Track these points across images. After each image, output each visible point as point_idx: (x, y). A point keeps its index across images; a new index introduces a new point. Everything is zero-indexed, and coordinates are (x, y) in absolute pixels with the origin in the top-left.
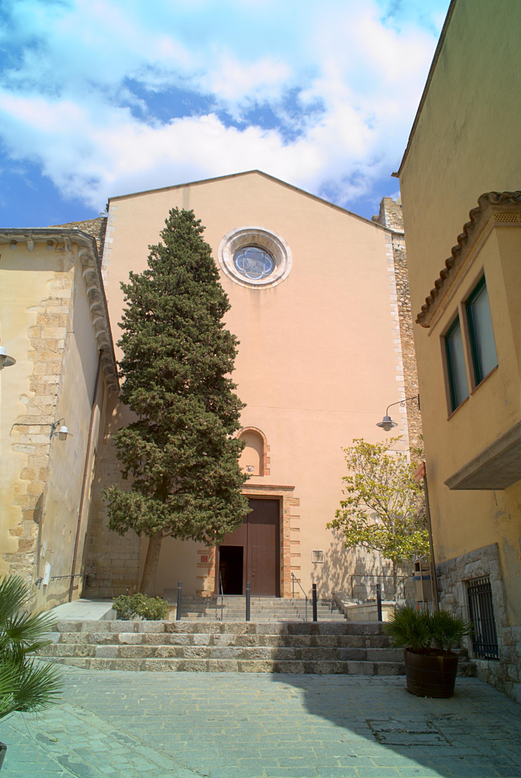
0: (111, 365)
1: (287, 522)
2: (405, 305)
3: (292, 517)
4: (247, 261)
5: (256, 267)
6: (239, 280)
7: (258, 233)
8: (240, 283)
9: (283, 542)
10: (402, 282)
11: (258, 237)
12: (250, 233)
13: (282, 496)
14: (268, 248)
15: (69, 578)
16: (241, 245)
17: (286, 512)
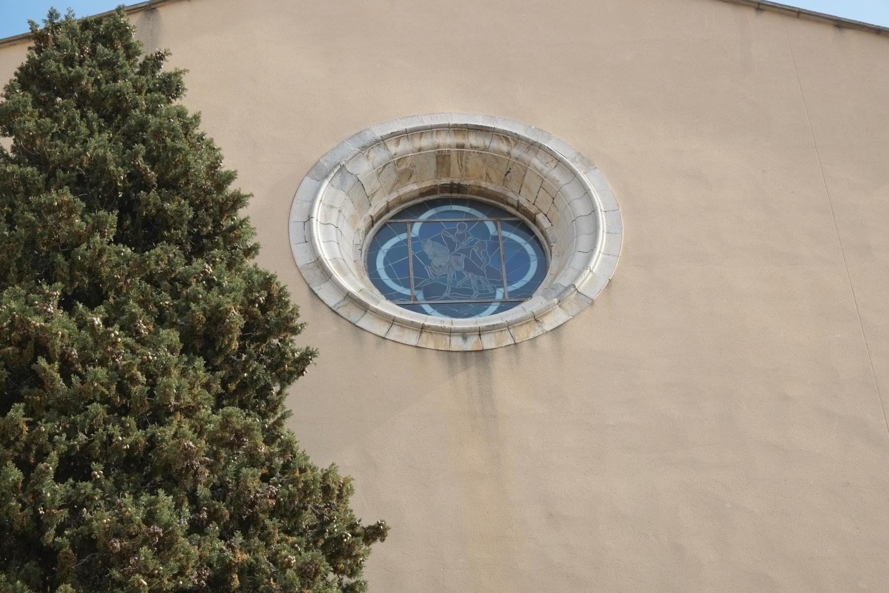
4: (424, 256)
6: (393, 321)
7: (459, 140)
8: (395, 334)
11: (460, 155)
12: (425, 142)
14: (512, 196)
16: (394, 195)
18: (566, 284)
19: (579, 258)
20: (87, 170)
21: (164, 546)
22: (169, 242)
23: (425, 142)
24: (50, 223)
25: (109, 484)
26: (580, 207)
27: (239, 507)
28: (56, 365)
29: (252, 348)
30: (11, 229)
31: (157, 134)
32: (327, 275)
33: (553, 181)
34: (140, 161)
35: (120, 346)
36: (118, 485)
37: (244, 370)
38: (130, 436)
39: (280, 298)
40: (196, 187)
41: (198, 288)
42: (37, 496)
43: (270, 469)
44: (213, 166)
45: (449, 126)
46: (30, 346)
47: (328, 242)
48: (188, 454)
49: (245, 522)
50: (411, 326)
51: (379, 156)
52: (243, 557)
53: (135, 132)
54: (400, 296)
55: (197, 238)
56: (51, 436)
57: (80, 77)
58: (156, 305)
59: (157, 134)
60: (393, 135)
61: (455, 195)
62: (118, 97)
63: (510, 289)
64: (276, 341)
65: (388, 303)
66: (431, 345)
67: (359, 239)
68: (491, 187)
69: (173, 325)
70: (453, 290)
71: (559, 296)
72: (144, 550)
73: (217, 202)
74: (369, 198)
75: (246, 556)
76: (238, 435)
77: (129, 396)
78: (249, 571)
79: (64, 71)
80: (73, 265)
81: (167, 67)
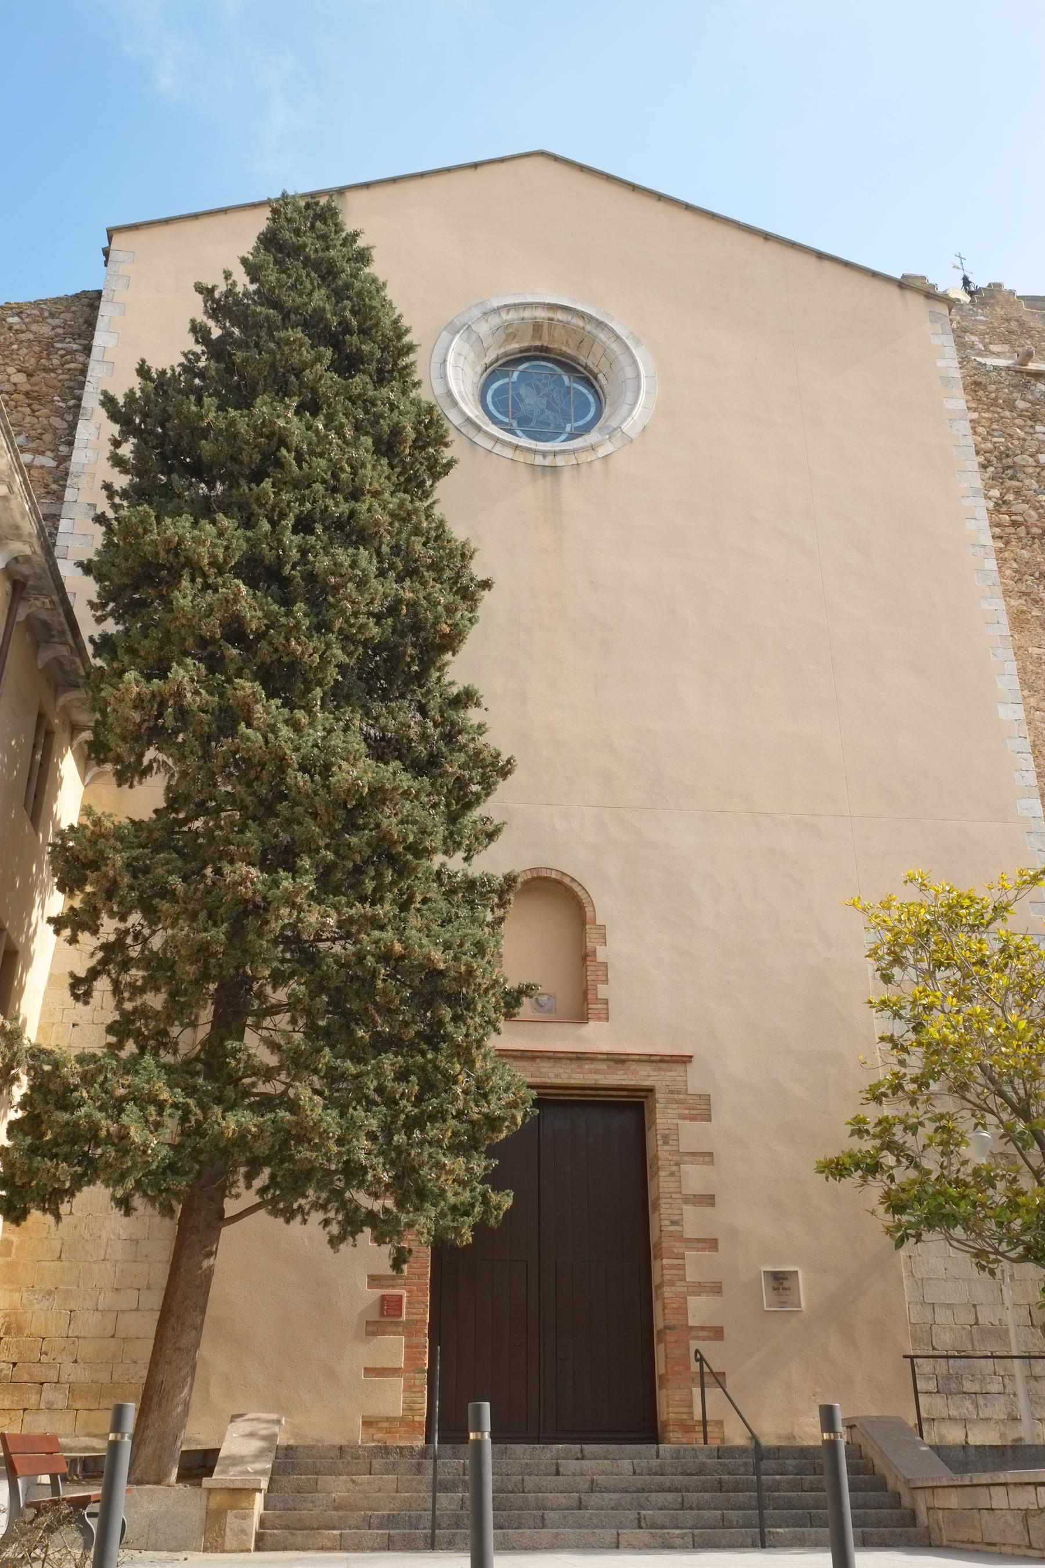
0: (64, 651)
1: (672, 1174)
2: (1004, 509)
3: (686, 1158)
4: (519, 395)
5: (548, 412)
6: (497, 440)
7: (550, 315)
8: (498, 449)
9: (659, 1243)
10: (990, 446)
11: (550, 325)
12: (527, 314)
13: (651, 1090)
14: (582, 359)
15: (1032, 1361)
16: (502, 351)
17: (666, 1143)
18: (615, 426)
19: (626, 408)
20: (310, 316)
21: (362, 584)
22: (364, 373)
23: (527, 314)
24: (287, 352)
25: (325, 538)
26: (629, 373)
27: (407, 562)
28: (293, 454)
29: (416, 451)
30: (260, 354)
31: (360, 294)
32: (455, 403)
33: (612, 351)
34: (347, 313)
35: (334, 445)
36: (331, 539)
37: (411, 469)
38: (339, 508)
39: (438, 421)
40: (383, 335)
41: (381, 408)
42: (280, 541)
43: (427, 538)
44: (396, 322)
45: (544, 304)
46: (276, 439)
47: (456, 379)
48: (377, 524)
49: (411, 572)
50: (504, 443)
51: (495, 321)
52: (409, 595)
53: (342, 290)
54: (501, 422)
55: (380, 371)
56: (289, 502)
57: (305, 246)
58: (354, 417)
59: (360, 294)
60: (505, 306)
61: (543, 354)
62: (331, 263)
63: (576, 425)
64: (431, 450)
65: (494, 427)
66: (521, 460)
67: (476, 379)
68: (569, 351)
69: (367, 434)
70: (537, 422)
71: (609, 434)
72: (349, 585)
73: (397, 348)
74: (486, 350)
75: (411, 595)
76: (409, 514)
77: (338, 481)
78: (412, 605)
79: (294, 240)
80: (302, 384)
81: (361, 243)
